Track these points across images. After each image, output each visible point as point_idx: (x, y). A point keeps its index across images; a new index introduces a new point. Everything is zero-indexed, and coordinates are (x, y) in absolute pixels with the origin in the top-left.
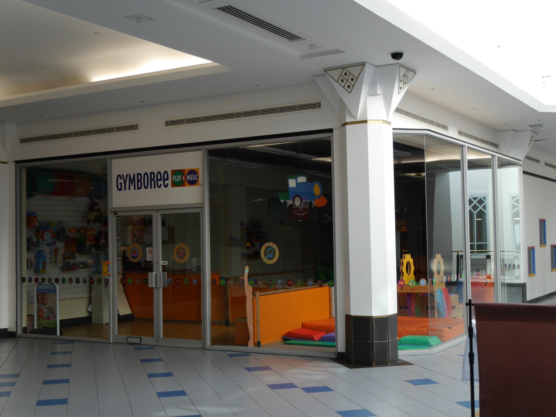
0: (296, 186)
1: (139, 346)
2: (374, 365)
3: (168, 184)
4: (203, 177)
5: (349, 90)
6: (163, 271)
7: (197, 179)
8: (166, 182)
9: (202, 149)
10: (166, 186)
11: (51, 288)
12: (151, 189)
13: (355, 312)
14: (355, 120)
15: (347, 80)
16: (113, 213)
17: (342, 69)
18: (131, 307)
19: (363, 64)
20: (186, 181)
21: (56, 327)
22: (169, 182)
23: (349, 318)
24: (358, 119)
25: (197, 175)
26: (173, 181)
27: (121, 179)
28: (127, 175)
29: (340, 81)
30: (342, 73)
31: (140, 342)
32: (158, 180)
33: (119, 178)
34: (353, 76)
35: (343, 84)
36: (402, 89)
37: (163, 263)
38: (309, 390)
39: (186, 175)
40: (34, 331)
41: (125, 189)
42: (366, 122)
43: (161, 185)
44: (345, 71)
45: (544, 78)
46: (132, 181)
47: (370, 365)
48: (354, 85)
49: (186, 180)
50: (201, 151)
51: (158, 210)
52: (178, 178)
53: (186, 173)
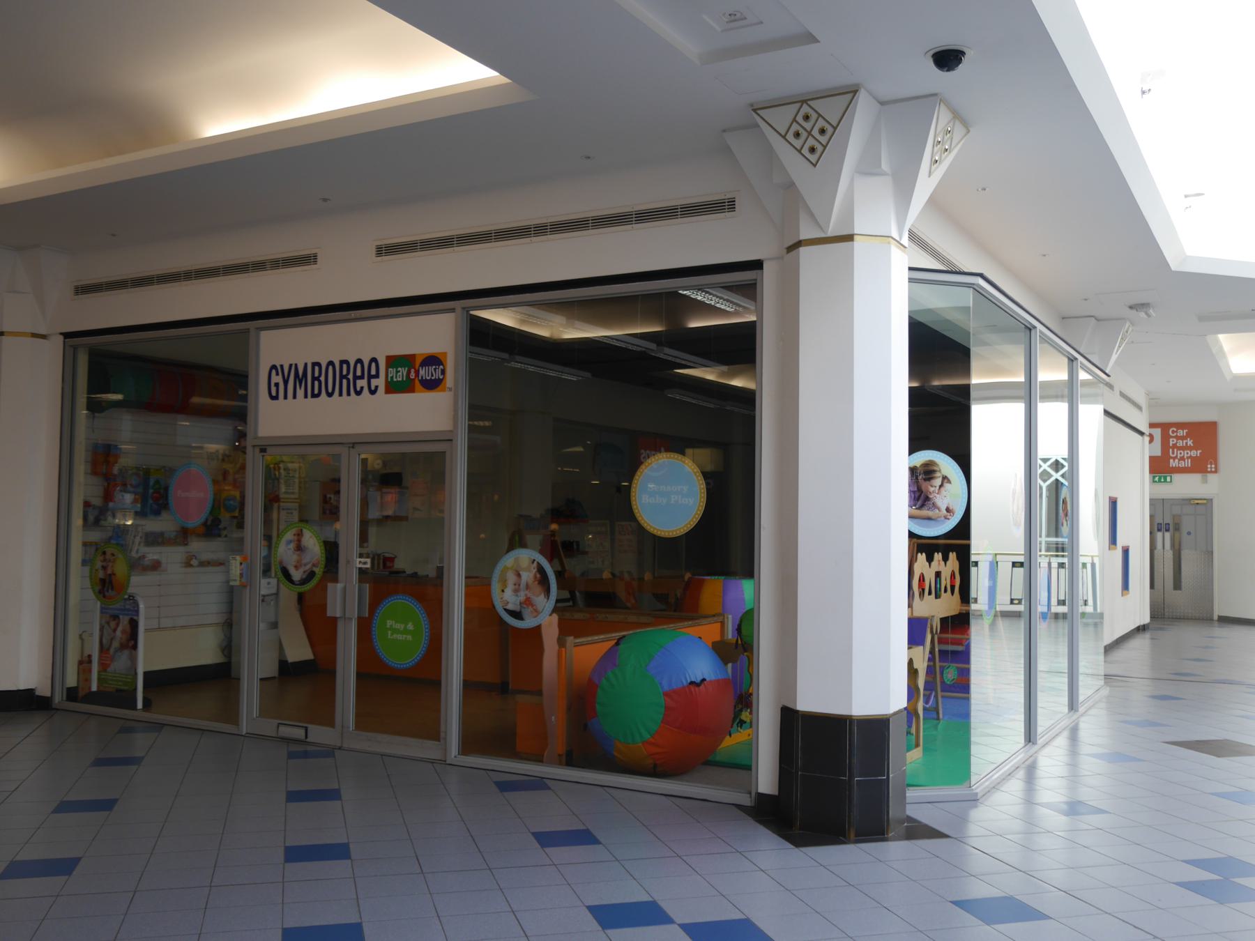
0: (1162, 454)
1: (301, 751)
2: (852, 836)
3: (377, 387)
4: (453, 373)
5: (813, 158)
6: (361, 581)
7: (441, 377)
8: (374, 382)
9: (454, 309)
10: (373, 392)
11: (127, 607)
12: (341, 398)
13: (807, 702)
14: (823, 235)
15: (810, 133)
16: (257, 450)
17: (800, 104)
18: (312, 645)
19: (853, 91)
20: (417, 382)
21: (135, 689)
22: (380, 382)
23: (789, 717)
24: (831, 231)
25: (441, 367)
26: (389, 380)
27: (277, 374)
28: (291, 366)
31: (304, 738)
32: (356, 378)
33: (274, 372)
35: (798, 143)
37: (360, 562)
39: (417, 367)
40: (91, 698)
41: (286, 397)
42: (849, 238)
43: (362, 388)
44: (805, 109)
45: (1188, 198)
46: (300, 379)
47: (844, 836)
48: (827, 145)
49: (417, 379)
50: (453, 314)
51: (354, 443)
52: (400, 373)
53: (418, 362)
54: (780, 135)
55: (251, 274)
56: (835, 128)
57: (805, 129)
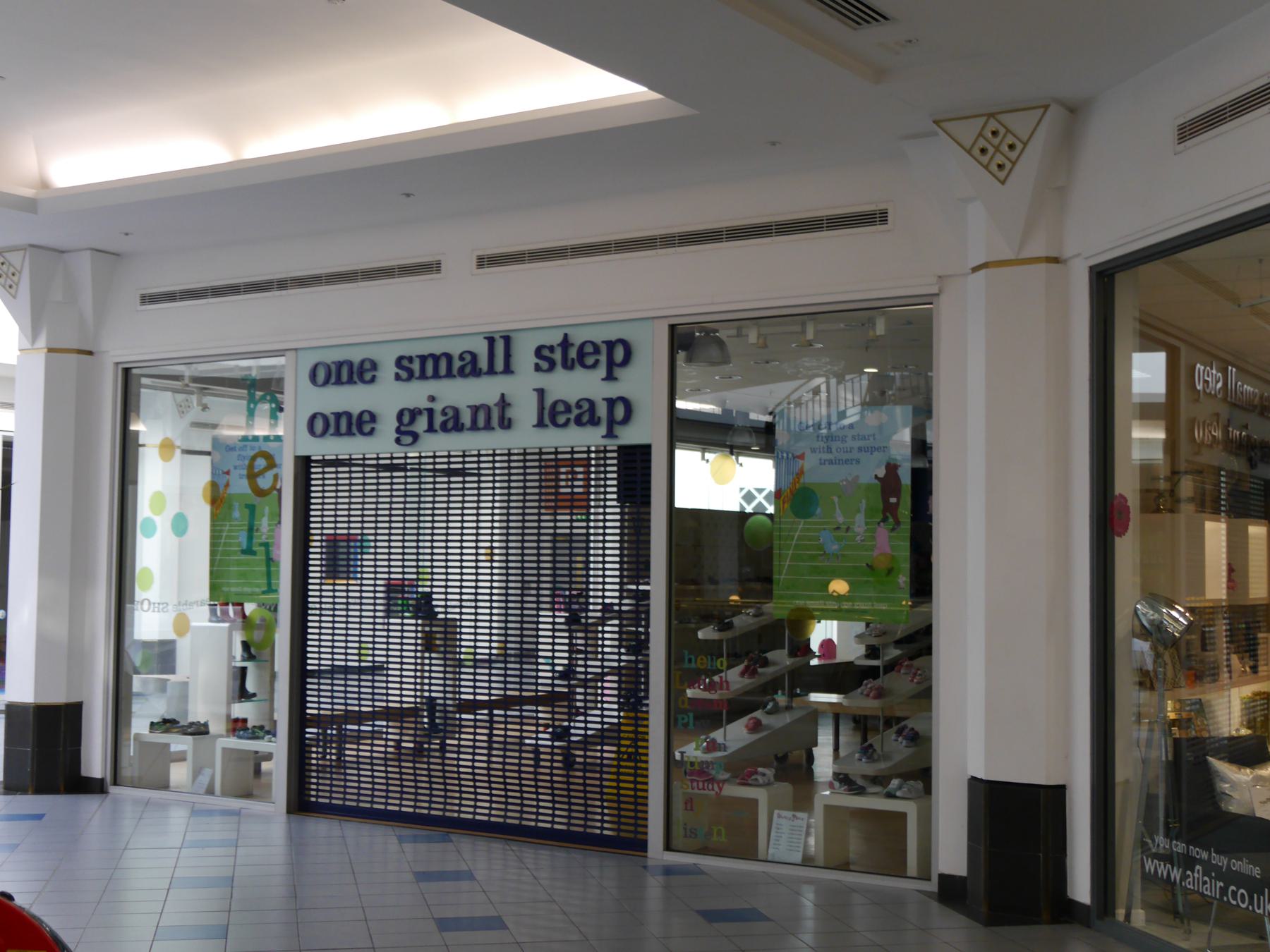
0: (1203, 525)
5: (1002, 175)
15: (997, 149)
54: (965, 150)
55: (359, 284)
56: (1025, 144)
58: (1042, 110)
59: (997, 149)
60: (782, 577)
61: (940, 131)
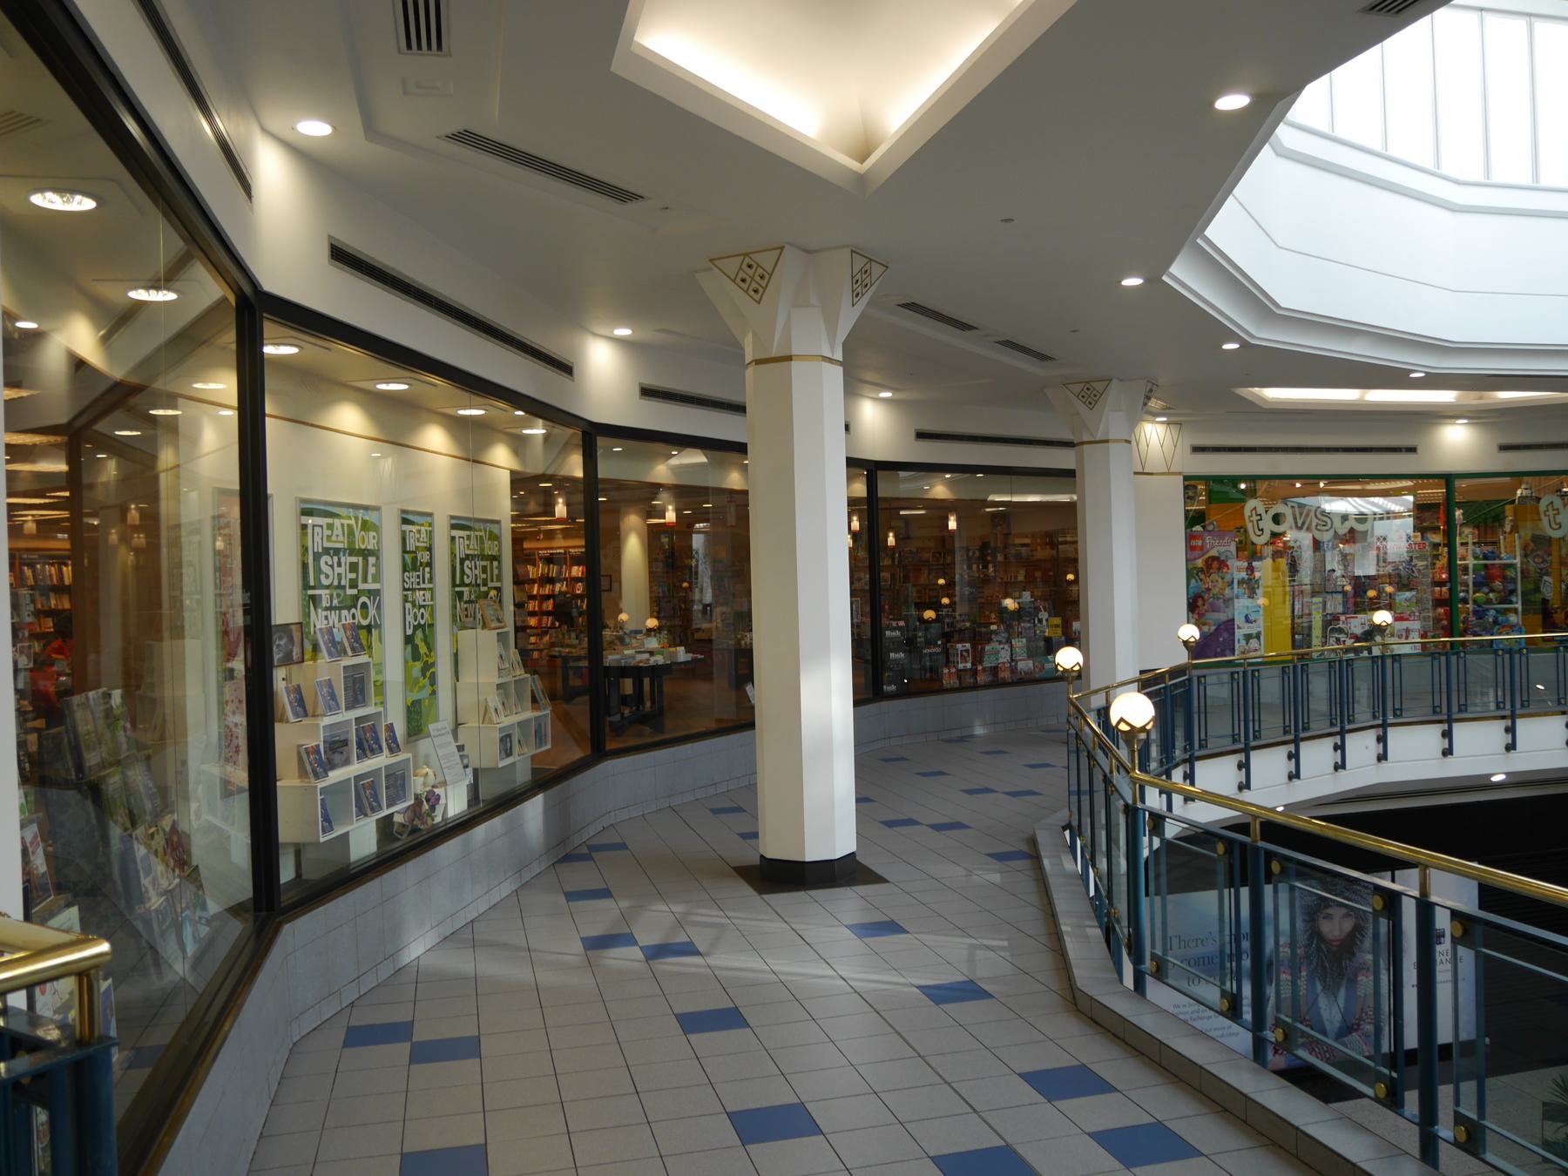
0: (584, 474)
5: (757, 297)
17: (742, 258)
29: (1080, 397)
30: (742, 264)
34: (763, 269)
35: (745, 286)
36: (860, 295)
38: (939, 827)
44: (1087, 386)
57: (761, 286)
58: (778, 251)
59: (752, 278)
60: (1431, 615)
61: (714, 268)
